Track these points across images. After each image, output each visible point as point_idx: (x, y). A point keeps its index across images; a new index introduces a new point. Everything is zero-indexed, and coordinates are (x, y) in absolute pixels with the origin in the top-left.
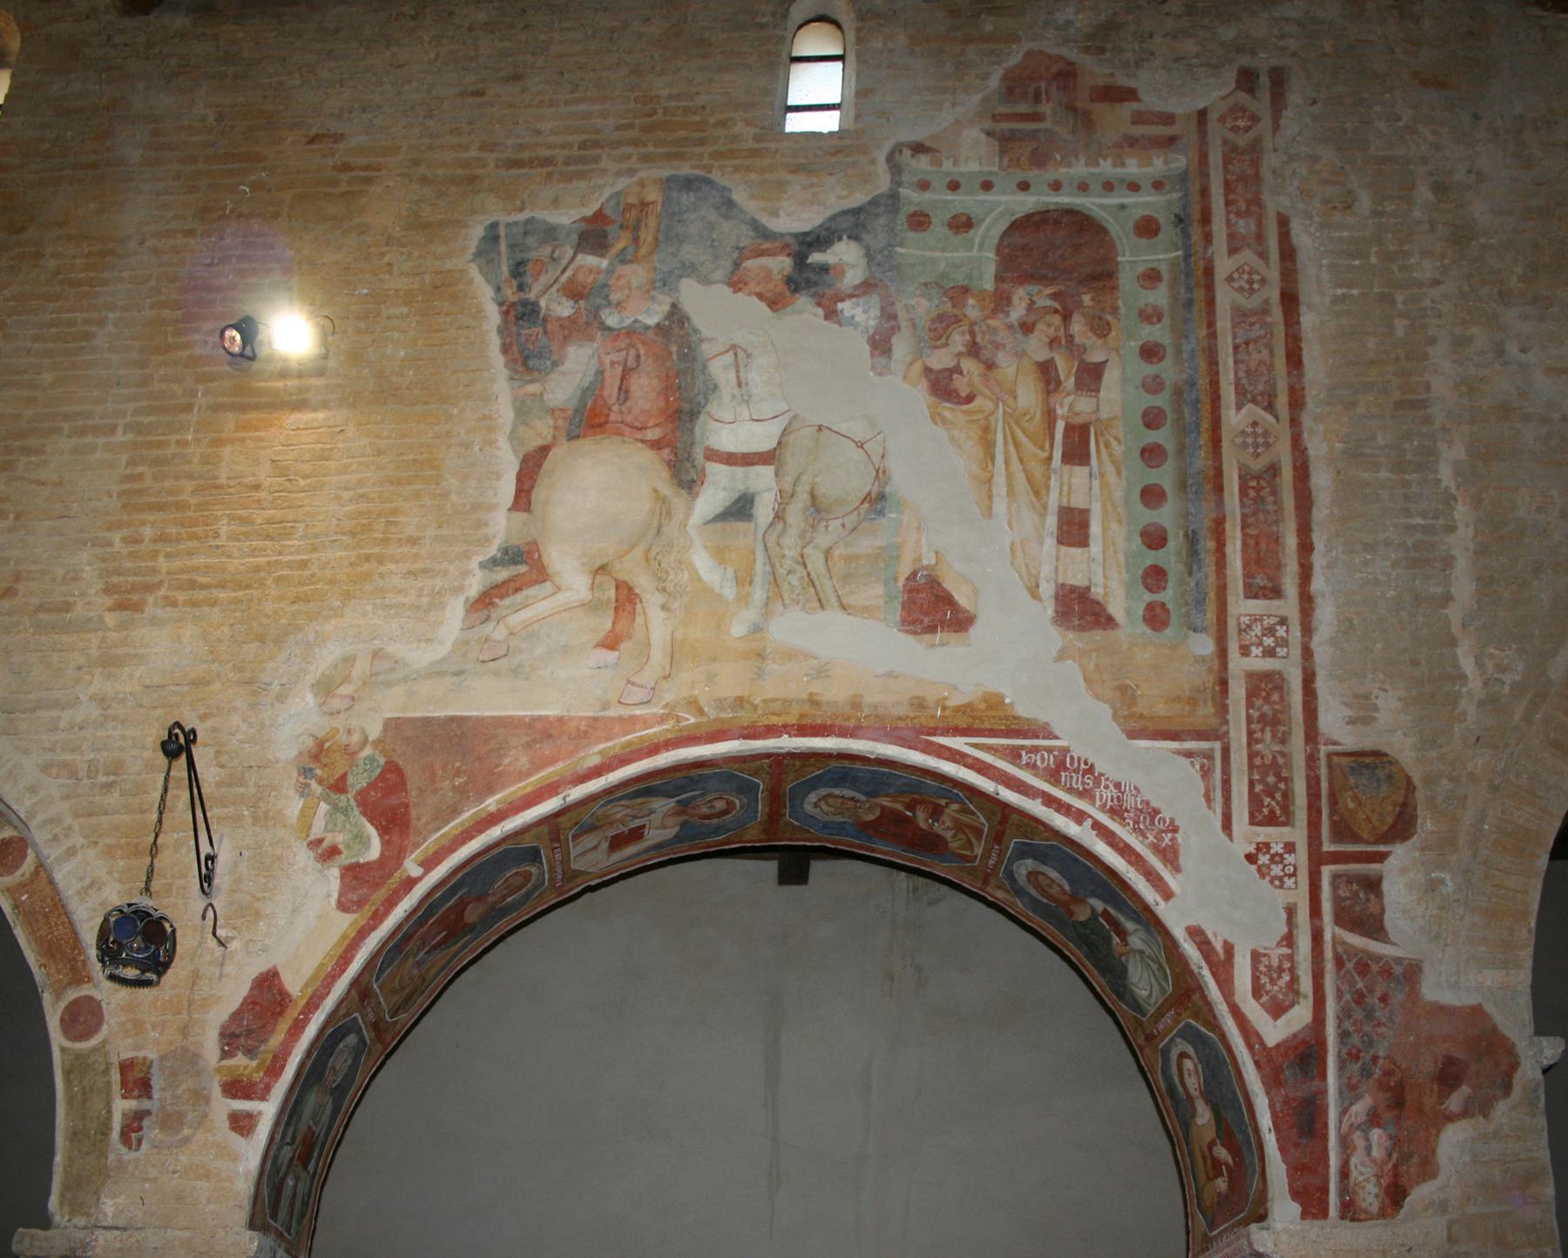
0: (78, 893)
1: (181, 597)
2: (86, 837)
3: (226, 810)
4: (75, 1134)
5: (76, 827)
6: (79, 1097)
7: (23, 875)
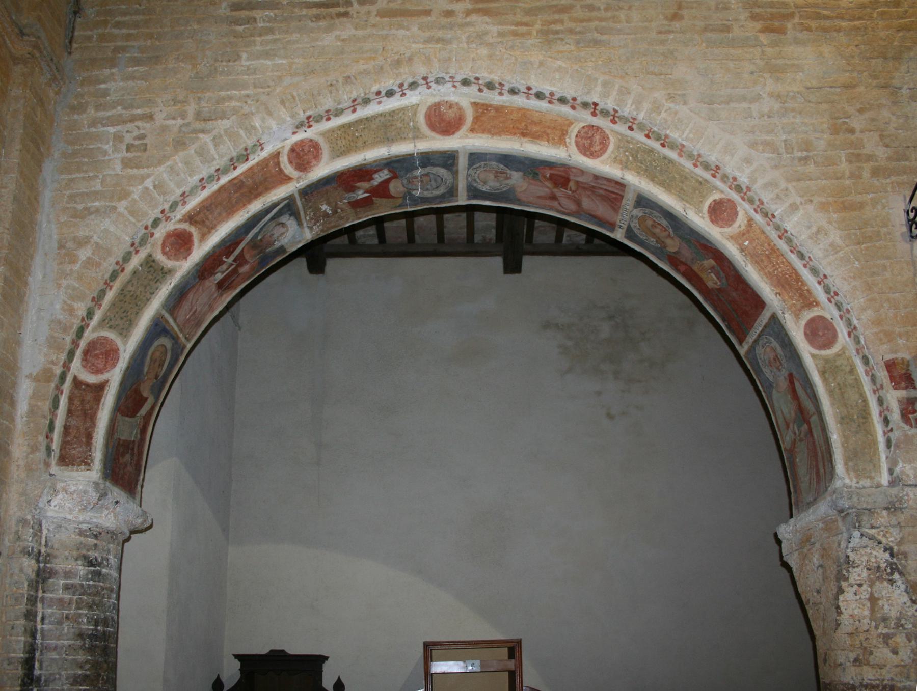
0: (810, 238)
1: (813, 24)
2: (802, 196)
3: (901, 178)
4: (842, 418)
5: (790, 188)
6: (837, 390)
7: (740, 226)
